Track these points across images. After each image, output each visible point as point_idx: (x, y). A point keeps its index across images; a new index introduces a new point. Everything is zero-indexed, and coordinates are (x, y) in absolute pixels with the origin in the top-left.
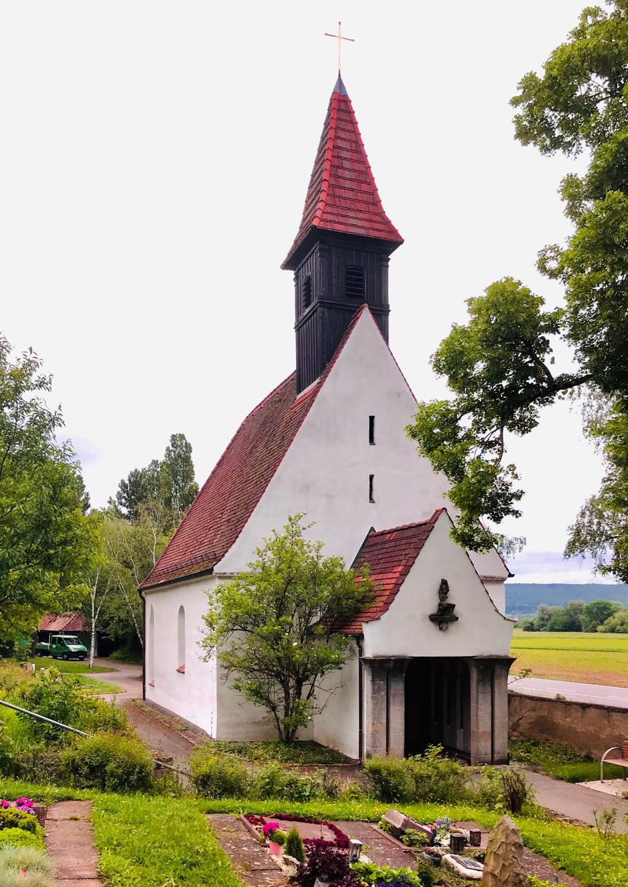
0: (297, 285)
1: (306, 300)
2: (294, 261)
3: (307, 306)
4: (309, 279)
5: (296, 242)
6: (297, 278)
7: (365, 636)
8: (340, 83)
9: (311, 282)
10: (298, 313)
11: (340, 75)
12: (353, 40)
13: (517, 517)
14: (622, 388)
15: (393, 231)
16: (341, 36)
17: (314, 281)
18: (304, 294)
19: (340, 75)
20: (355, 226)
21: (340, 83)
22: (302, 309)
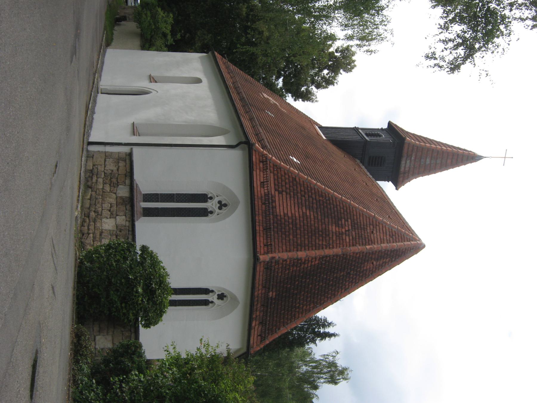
0: (378, 129)
1: (369, 134)
2: (392, 128)
3: (367, 135)
4: (380, 136)
5: (392, 203)
6: (382, 129)
7: (390, 270)
8: (479, 158)
9: (378, 137)
10: (362, 129)
11: (486, 157)
12: (504, 165)
13: (179, 352)
14: (312, 383)
15: (403, 183)
16: (504, 157)
17: (378, 138)
18: (372, 133)
19: (486, 157)
20: (405, 164)
21: (479, 158)
22: (365, 132)
